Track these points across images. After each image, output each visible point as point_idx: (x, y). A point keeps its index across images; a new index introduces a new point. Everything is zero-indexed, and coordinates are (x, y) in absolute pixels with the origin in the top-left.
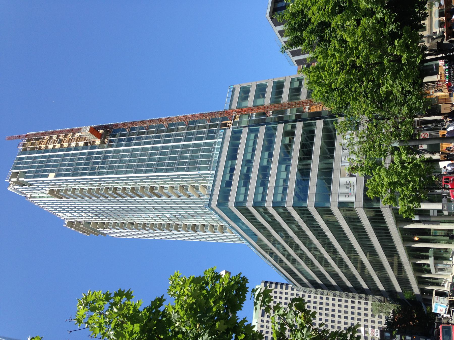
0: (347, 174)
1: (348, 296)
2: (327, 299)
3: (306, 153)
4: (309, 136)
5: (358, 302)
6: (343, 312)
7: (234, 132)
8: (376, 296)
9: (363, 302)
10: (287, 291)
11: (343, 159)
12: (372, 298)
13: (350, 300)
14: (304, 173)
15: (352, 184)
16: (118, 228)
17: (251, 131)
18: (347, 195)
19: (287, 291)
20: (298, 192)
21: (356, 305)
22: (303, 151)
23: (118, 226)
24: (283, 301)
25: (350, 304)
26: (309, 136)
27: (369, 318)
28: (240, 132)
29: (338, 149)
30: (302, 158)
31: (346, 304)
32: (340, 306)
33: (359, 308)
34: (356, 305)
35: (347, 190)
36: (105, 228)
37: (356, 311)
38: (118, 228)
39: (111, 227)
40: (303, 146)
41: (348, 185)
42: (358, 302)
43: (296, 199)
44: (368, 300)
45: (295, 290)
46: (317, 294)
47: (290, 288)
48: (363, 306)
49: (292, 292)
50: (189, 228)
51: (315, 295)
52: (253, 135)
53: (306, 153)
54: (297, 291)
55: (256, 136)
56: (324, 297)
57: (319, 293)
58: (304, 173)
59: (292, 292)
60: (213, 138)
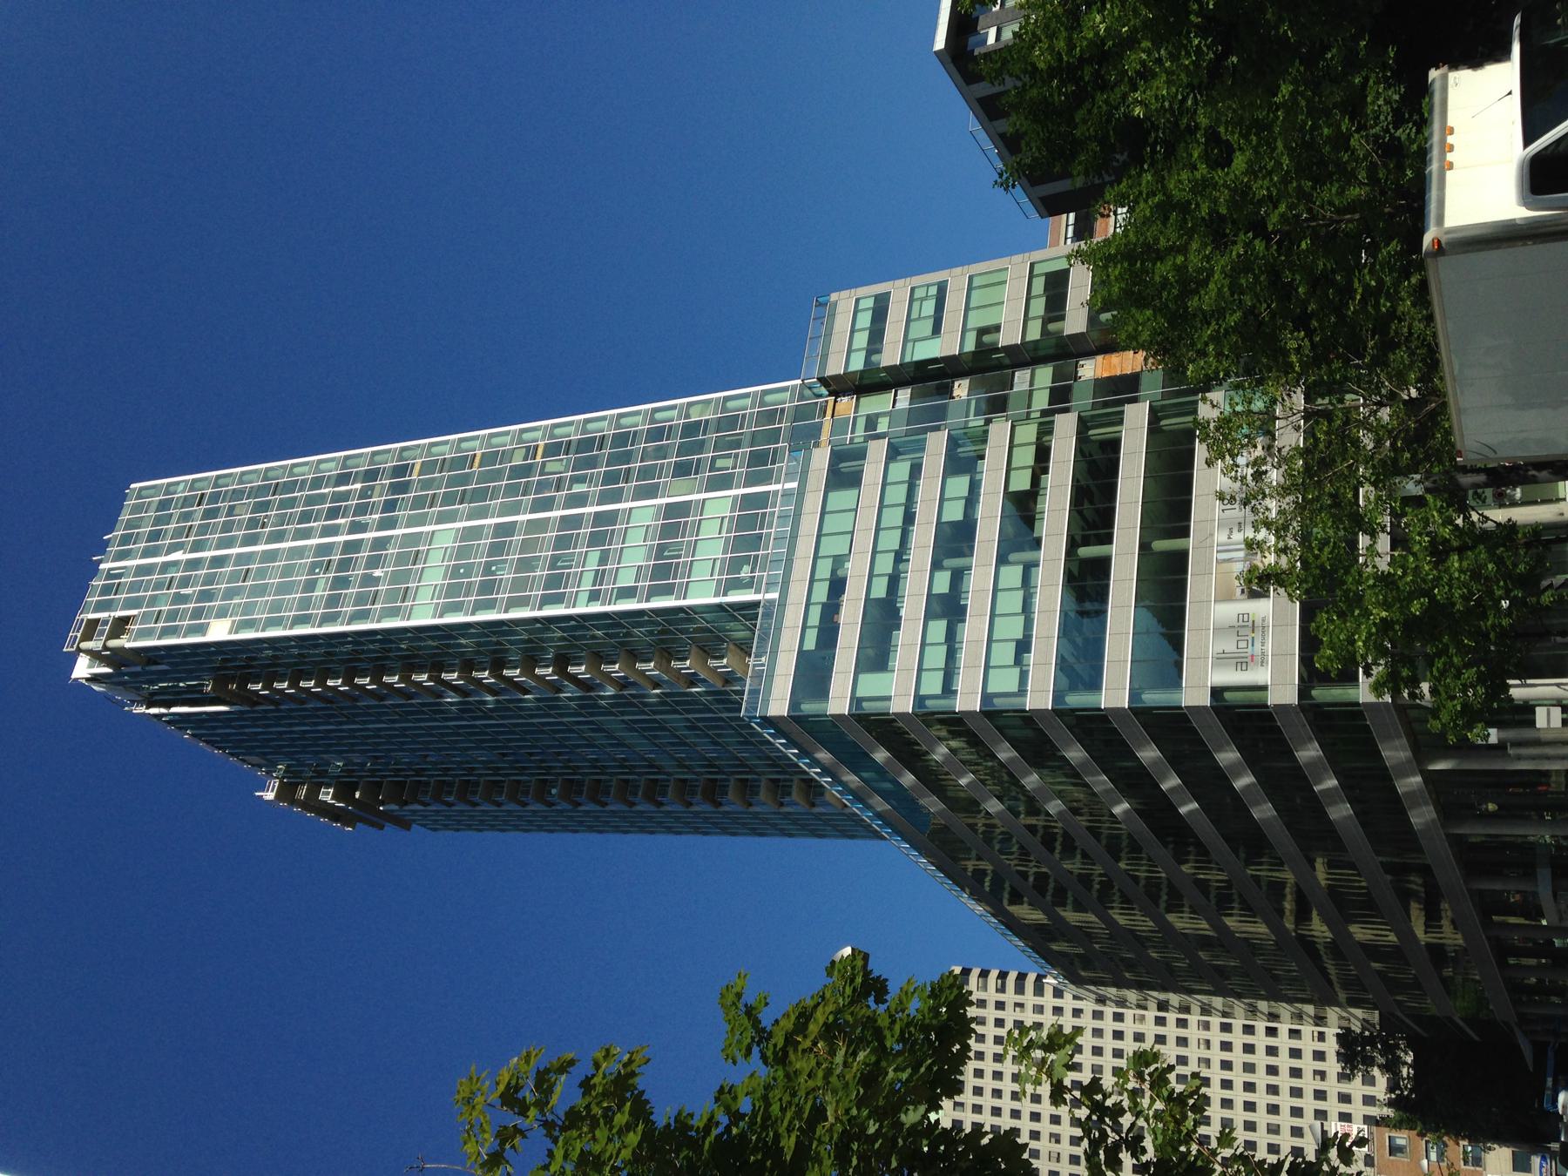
0: (1239, 591)
1: (1253, 1011)
2: (1248, 1030)
3: (1092, 510)
4: (1097, 466)
5: (1291, 1031)
6: (1238, 1067)
7: (837, 457)
8: (1352, 1010)
9: (1308, 1030)
10: (1039, 1000)
11: (1221, 537)
12: (1341, 1018)
13: (1261, 1026)
14: (1087, 582)
15: (1258, 623)
16: (451, 799)
17: (893, 453)
18: (1242, 663)
19: (1039, 1000)
20: (1071, 660)
21: (1283, 1042)
22: (1080, 513)
23: (450, 793)
24: (988, 1066)
25: (1261, 1040)
26: (1097, 466)
27: (1332, 1086)
28: (861, 454)
29: (1204, 507)
30: (1078, 538)
31: (1249, 1039)
32: (1249, 1049)
33: (1272, 1051)
34: (1283, 1042)
35: (1242, 644)
36: (406, 803)
37: (1284, 1062)
38: (451, 799)
39: (427, 799)
40: (1081, 495)
41: (1247, 628)
42: (1291, 1031)
43: (1065, 681)
44: (1325, 1025)
45: (1068, 996)
46: (1145, 1008)
47: (1049, 991)
48: (1308, 1044)
49: (1058, 1002)
50: (694, 793)
51: (1098, 1008)
52: (901, 470)
53: (1092, 510)
54: (1075, 998)
55: (916, 470)
56: (1172, 1017)
57: (1152, 1005)
58: (1087, 582)
59: (1058, 1002)
60: (766, 478)
